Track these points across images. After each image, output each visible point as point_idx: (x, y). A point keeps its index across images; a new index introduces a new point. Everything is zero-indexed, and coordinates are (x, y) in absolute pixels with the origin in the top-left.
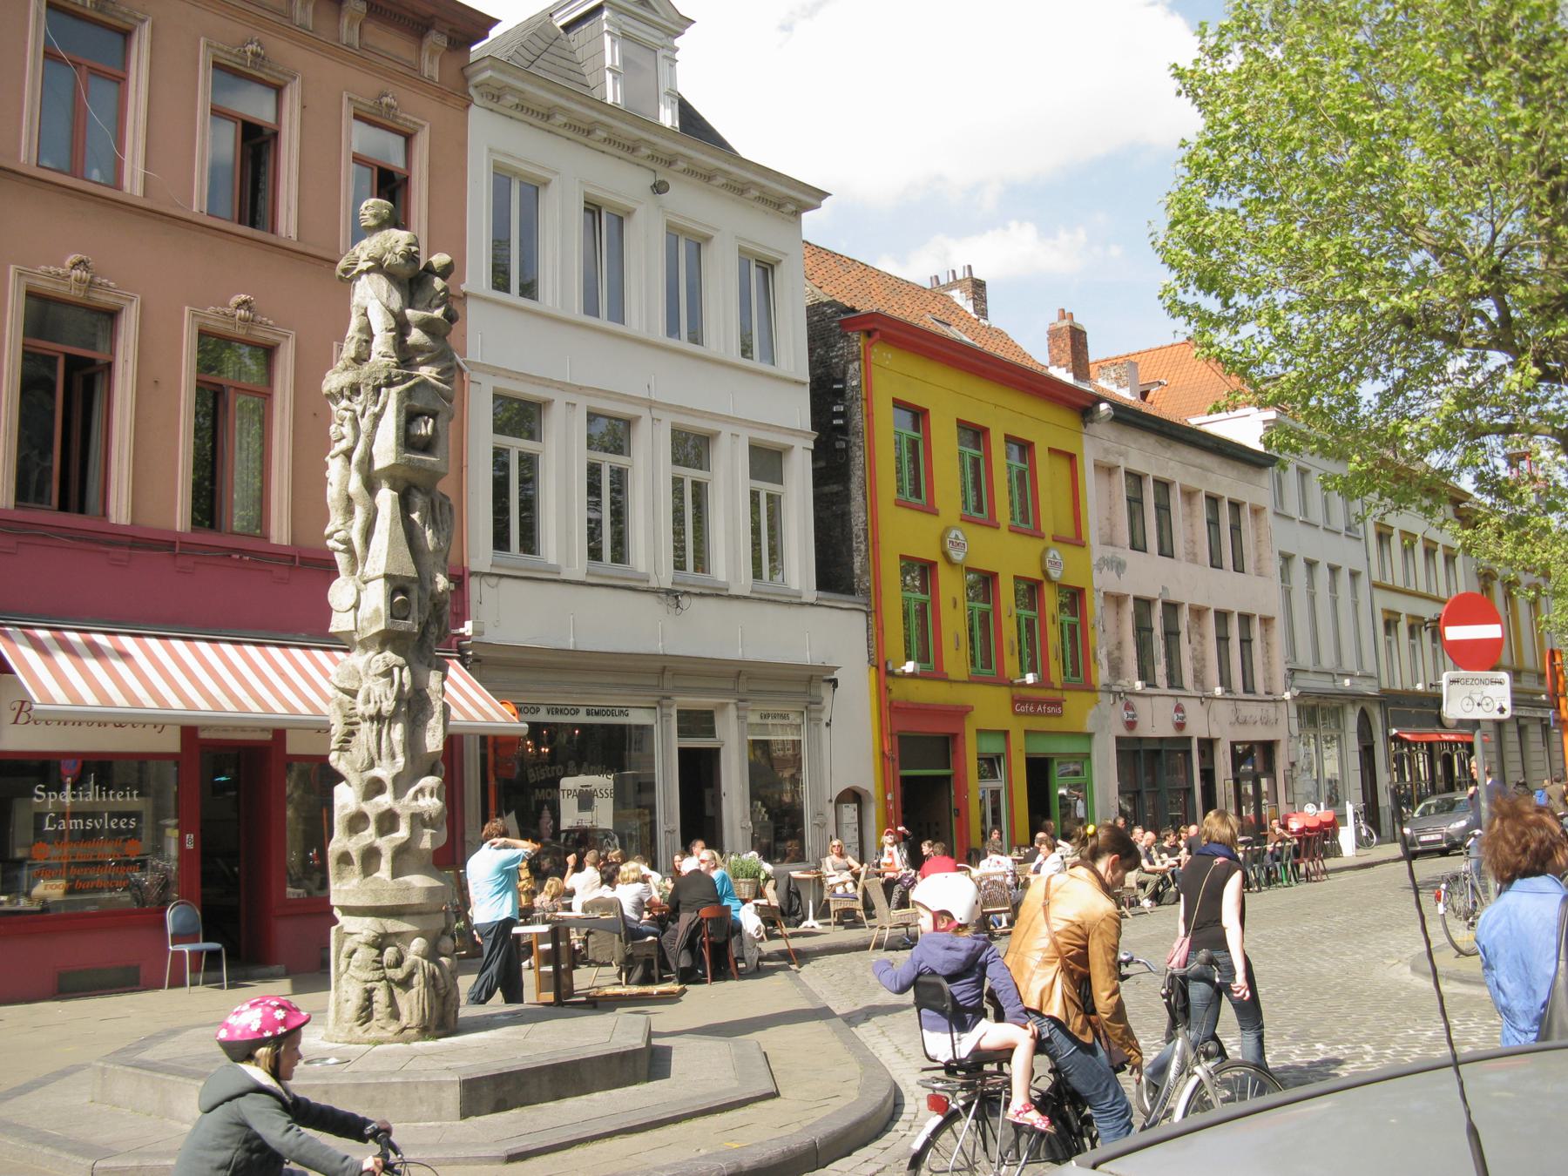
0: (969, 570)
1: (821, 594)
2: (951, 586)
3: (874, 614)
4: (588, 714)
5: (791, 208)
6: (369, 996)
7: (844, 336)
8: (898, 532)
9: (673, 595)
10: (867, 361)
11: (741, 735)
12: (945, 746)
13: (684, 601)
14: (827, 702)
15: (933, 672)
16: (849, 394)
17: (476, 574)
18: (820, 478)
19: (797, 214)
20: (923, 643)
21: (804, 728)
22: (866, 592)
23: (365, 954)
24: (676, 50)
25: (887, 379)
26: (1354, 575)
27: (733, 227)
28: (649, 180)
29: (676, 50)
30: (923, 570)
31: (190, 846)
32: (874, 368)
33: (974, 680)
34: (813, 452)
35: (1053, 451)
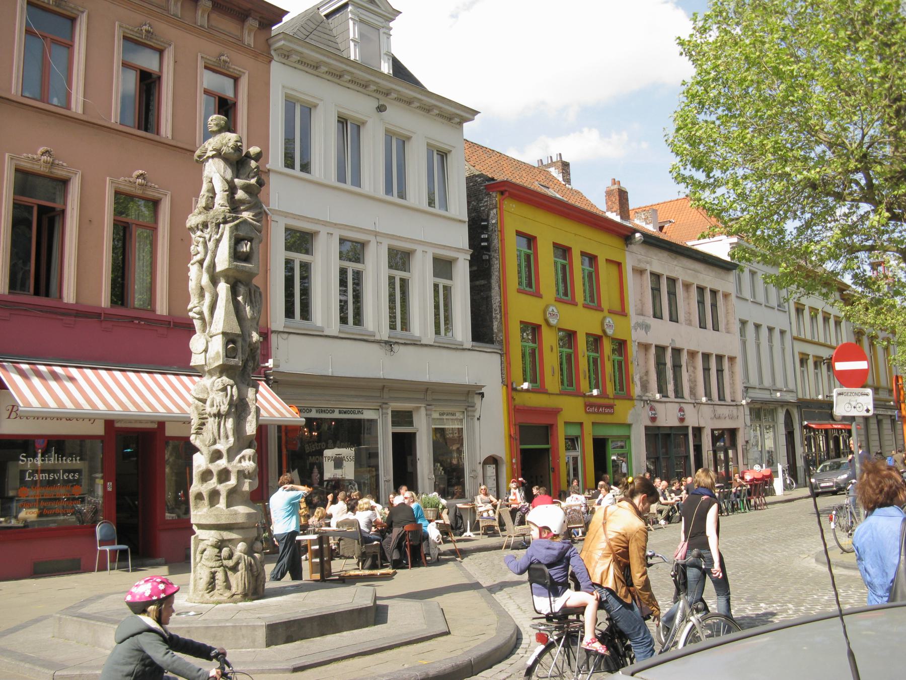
0: (560, 330)
1: (474, 343)
2: (549, 339)
3: (505, 355)
4: (340, 413)
5: (457, 120)
6: (213, 576)
7: (488, 194)
8: (519, 308)
9: (389, 344)
10: (501, 209)
11: (428, 425)
12: (546, 431)
13: (395, 347)
14: (478, 406)
15: (539, 389)
16: (490, 228)
17: (275, 332)
18: (474, 276)
19: (460, 124)
20: (534, 372)
21: (465, 421)
22: (501, 342)
23: (211, 552)
24: (391, 29)
25: (513, 219)
26: (782, 332)
27: (423, 131)
28: (375, 104)
29: (391, 29)
30: (533, 330)
31: (110, 489)
32: (505, 213)
33: (563, 393)
34: (470, 261)
35: (608, 261)
